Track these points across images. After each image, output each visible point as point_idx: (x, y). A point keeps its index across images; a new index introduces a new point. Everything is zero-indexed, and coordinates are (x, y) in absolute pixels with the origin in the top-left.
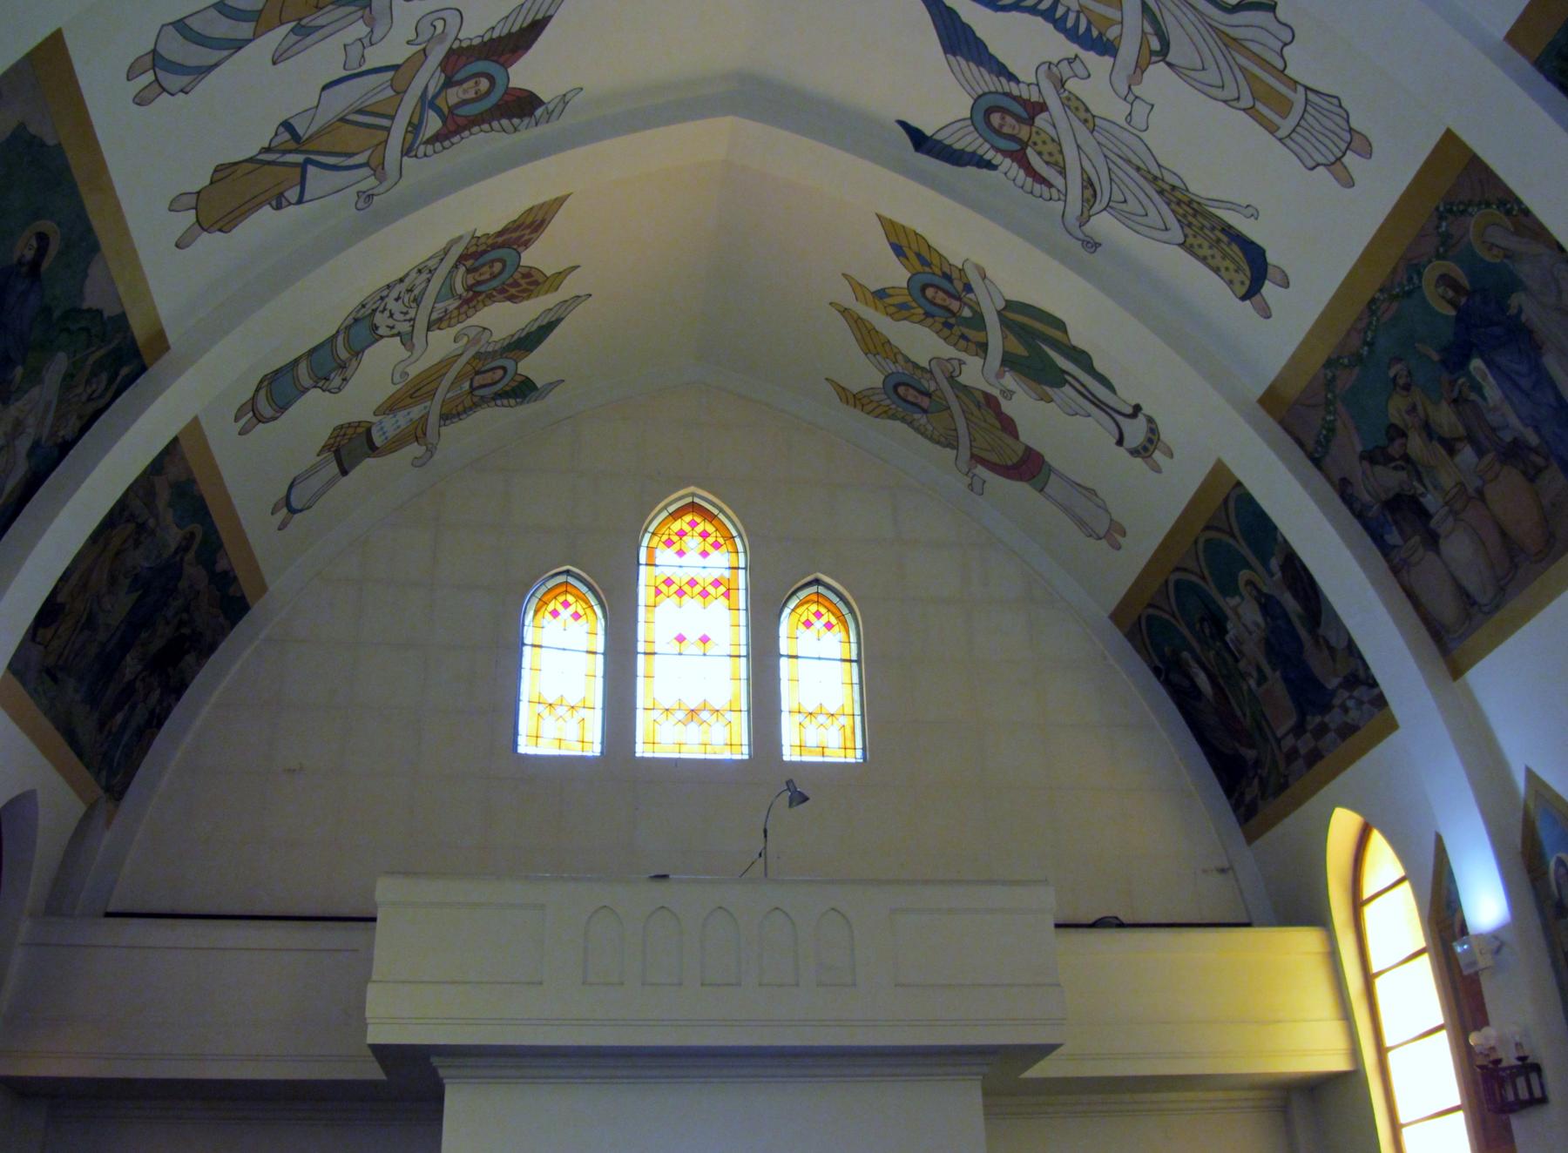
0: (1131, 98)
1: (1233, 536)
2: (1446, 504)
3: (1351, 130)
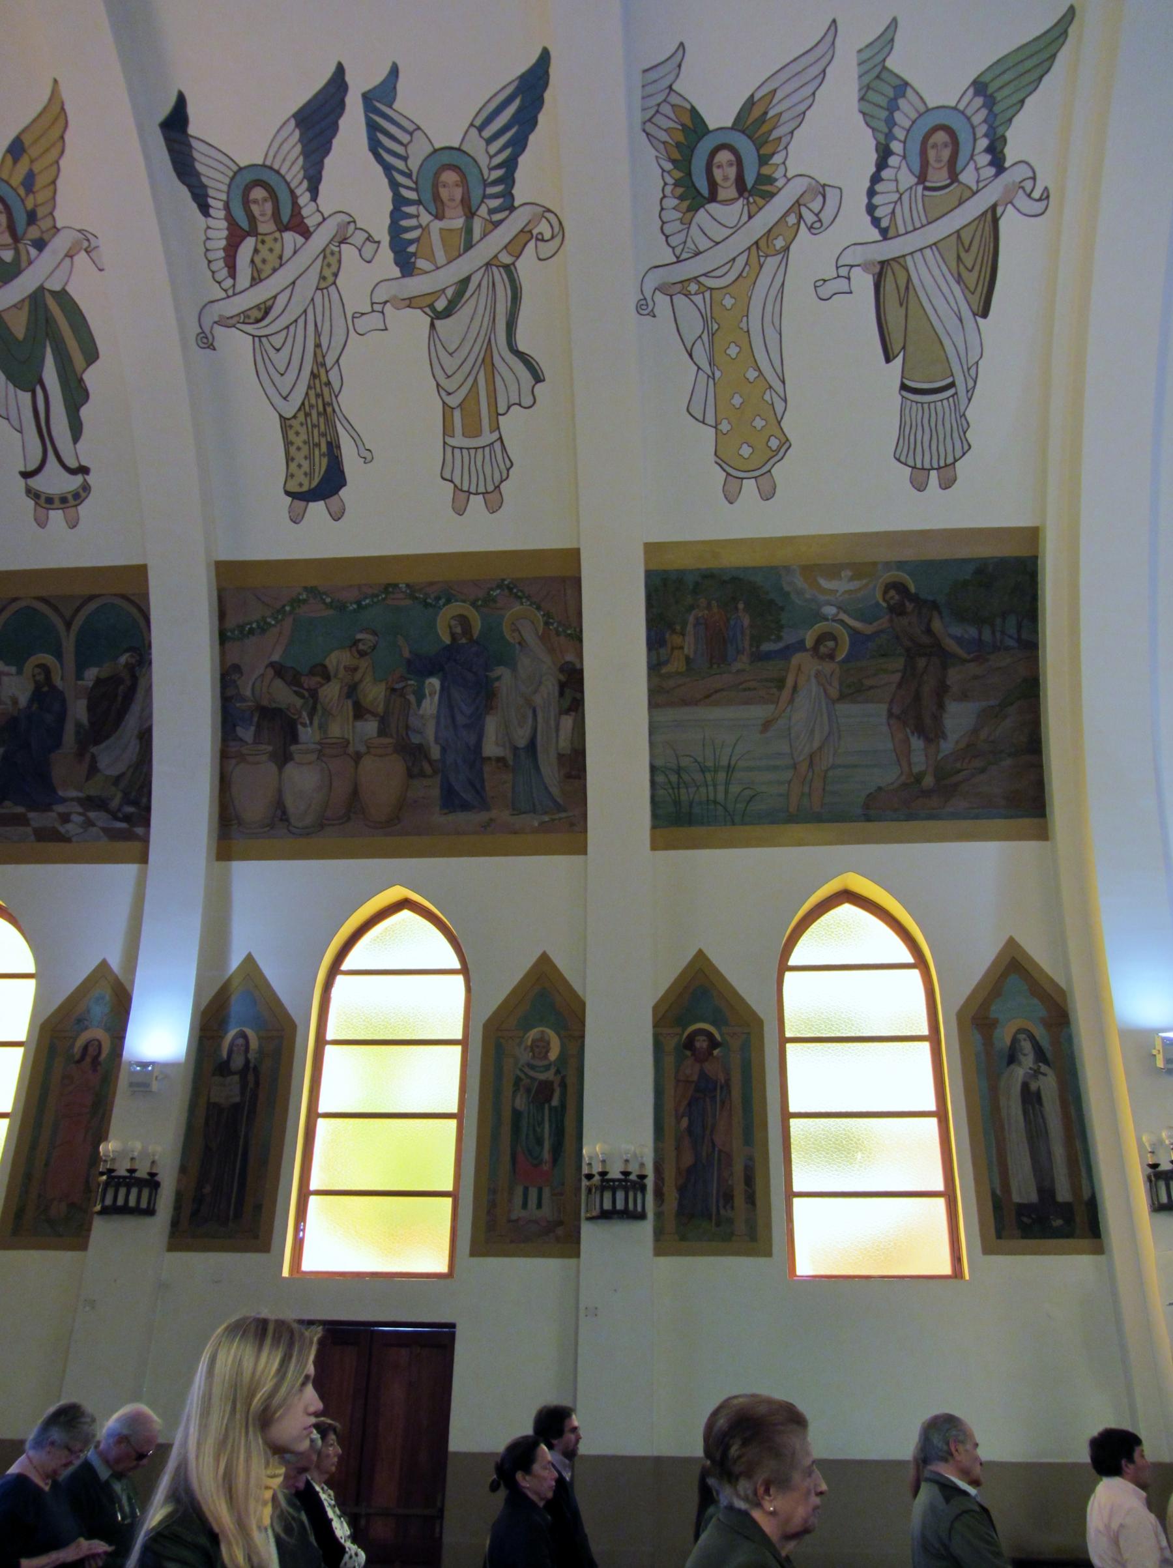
0: (378, 307)
1: (68, 625)
2: (320, 743)
3: (498, 487)
